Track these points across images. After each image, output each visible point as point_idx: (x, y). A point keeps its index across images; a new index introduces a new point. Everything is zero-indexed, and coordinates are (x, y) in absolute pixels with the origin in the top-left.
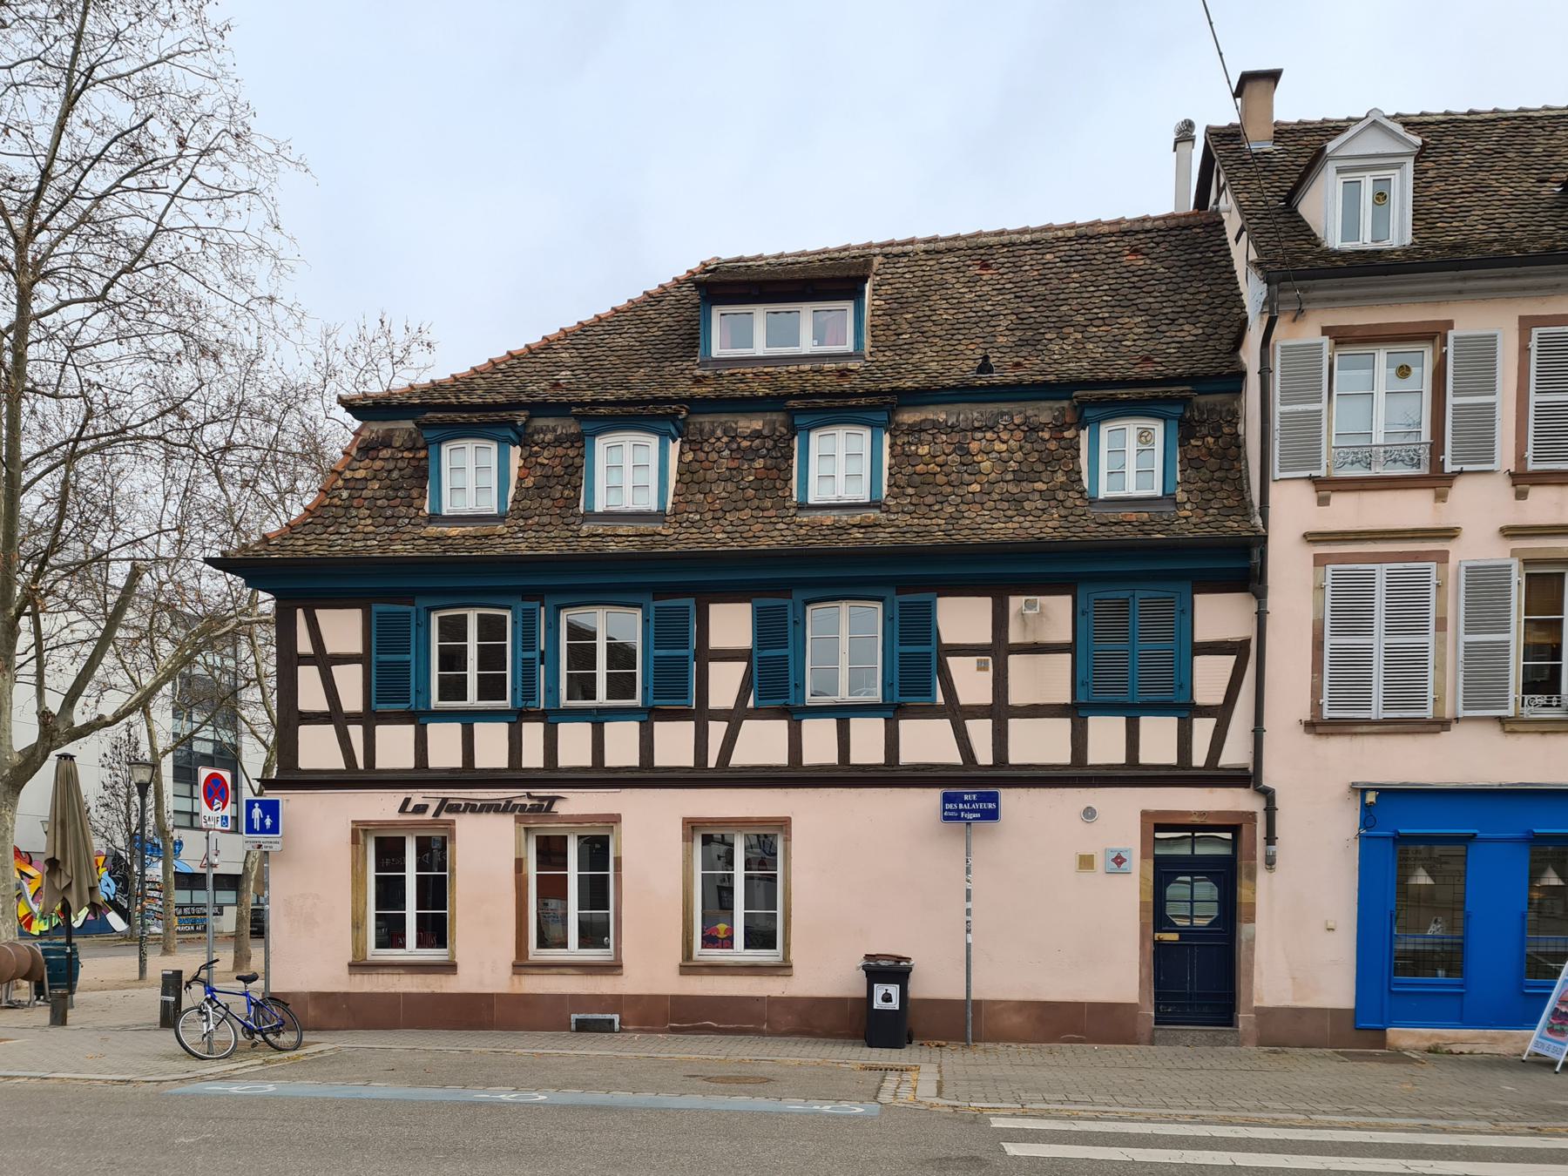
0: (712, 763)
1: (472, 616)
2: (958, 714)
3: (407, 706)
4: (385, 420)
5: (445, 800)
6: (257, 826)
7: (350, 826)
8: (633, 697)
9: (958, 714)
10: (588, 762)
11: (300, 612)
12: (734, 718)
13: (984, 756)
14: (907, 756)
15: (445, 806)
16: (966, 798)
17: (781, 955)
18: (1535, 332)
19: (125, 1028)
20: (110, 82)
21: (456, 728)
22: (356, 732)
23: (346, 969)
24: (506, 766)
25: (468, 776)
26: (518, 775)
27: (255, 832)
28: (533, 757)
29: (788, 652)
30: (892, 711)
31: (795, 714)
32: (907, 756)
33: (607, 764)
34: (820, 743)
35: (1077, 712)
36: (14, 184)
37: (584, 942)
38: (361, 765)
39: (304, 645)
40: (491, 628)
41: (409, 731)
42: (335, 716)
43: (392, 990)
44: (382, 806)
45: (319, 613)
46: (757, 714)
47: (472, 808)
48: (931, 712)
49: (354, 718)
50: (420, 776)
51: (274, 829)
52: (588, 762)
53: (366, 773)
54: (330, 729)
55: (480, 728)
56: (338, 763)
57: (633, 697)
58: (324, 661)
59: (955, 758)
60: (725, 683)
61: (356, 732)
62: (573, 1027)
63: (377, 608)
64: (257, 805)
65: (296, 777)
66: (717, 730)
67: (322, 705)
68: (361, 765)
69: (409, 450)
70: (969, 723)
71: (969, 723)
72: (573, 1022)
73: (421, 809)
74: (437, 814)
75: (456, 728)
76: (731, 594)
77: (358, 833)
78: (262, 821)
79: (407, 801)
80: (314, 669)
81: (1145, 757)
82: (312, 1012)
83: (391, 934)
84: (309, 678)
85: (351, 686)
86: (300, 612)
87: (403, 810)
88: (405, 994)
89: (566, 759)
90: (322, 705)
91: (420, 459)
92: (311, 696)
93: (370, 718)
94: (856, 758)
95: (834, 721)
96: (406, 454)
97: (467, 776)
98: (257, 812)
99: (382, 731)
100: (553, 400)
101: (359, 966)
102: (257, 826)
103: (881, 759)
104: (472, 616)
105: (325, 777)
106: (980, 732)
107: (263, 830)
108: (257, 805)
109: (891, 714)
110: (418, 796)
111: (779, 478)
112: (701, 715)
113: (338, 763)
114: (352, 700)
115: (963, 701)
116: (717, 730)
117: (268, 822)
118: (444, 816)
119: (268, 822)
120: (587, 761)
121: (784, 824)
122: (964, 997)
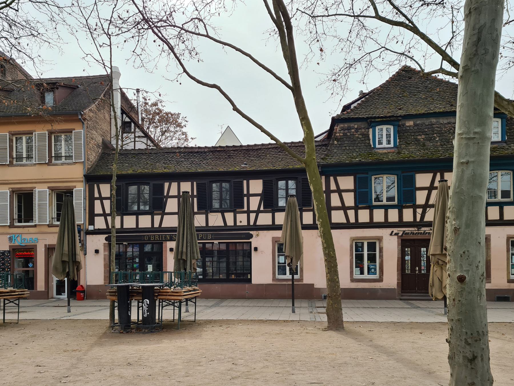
0: (418, 219)
5: (404, 231)
8: (395, 201)
9: (248, 212)
10: (271, 224)
13: (352, 220)
14: (506, 217)
17: (299, 277)
19: (232, 306)
21: (383, 211)
22: (109, 218)
26: (208, 228)
29: (402, 189)
30: (400, 208)
31: (371, 208)
32: (506, 217)
34: (379, 216)
36: (451, 47)
42: (344, 208)
45: (338, 178)
46: (262, 212)
52: (271, 224)
55: (390, 211)
56: (344, 221)
57: (395, 201)
58: (101, 199)
60: (254, 203)
61: (109, 218)
62: (323, 298)
63: (358, 176)
66: (419, 211)
67: (339, 204)
70: (348, 211)
71: (348, 211)
75: (383, 211)
79: (392, 232)
81: (360, 221)
84: (97, 203)
85: (349, 199)
89: (390, 220)
90: (339, 204)
93: (356, 208)
95: (384, 210)
103: (312, 223)
106: (351, 213)
111: (359, 143)
112: (415, 207)
113: (344, 221)
114: (108, 211)
116: (419, 211)
120: (271, 223)
121: (380, 239)
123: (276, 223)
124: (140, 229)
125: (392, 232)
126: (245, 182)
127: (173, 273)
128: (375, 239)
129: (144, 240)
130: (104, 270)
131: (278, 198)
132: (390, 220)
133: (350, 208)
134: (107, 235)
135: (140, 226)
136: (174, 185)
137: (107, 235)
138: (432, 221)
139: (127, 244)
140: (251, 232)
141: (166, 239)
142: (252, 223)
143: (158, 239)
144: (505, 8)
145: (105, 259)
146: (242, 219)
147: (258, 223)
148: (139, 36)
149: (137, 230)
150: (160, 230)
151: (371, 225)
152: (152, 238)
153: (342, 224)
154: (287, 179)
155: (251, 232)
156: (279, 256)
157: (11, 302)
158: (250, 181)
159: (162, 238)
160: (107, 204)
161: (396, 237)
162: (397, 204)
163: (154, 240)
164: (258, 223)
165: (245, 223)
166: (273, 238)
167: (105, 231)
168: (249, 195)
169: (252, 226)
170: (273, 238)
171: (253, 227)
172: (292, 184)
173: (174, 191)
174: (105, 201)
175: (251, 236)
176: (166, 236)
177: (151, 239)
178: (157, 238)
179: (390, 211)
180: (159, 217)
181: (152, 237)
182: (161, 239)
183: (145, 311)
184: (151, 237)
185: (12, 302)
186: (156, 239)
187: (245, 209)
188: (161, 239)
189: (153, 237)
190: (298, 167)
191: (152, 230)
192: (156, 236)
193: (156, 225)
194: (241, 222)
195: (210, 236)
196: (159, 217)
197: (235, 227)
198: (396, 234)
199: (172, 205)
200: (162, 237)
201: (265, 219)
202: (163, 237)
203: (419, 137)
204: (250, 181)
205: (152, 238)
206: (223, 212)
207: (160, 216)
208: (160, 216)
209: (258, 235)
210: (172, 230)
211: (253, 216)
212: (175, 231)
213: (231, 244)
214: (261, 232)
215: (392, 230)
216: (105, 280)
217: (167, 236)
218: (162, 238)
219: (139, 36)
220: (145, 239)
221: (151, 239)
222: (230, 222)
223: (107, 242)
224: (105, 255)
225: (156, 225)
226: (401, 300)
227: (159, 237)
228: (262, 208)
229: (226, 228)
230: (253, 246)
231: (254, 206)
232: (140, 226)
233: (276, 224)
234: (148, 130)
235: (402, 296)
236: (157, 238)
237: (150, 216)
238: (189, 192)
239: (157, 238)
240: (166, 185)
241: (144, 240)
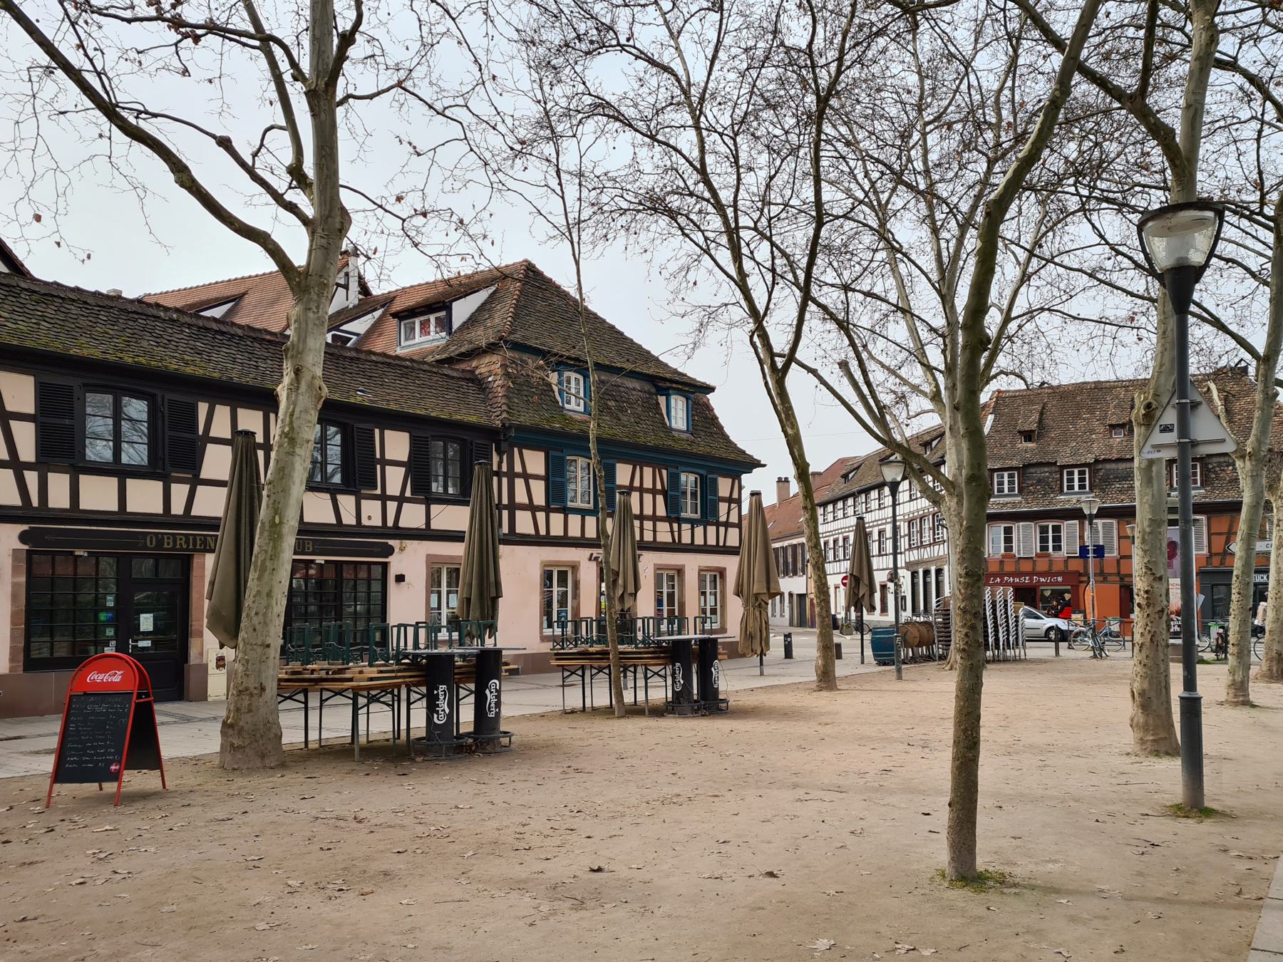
2: (384, 498)
9: (384, 498)
12: (401, 500)
16: (1060, 579)
18: (1065, 471)
20: (776, 252)
22: (31, 478)
26: (77, 515)
28: (591, 532)
31: (566, 511)
33: (128, 510)
35: (196, 481)
38: (35, 503)
39: (518, 468)
42: (532, 508)
46: (409, 500)
48: (375, 497)
58: (526, 477)
59: (17, 501)
60: (395, 479)
67: (526, 501)
68: (35, 503)
77: (439, 571)
79: (592, 555)
80: (522, 480)
86: (516, 449)
89: (520, 529)
90: (526, 501)
93: (548, 509)
97: (692, 547)
114: (540, 499)
115: (398, 494)
116: (722, 529)
123: (83, 506)
124: (435, 533)
125: (592, 555)
126: (377, 431)
127: (651, 621)
128: (551, 566)
129: (145, 547)
130: (12, 629)
131: (85, 437)
133: (29, 466)
134: (25, 527)
135: (131, 508)
136: (222, 413)
137: (25, 527)
138: (220, 519)
139: (86, 555)
140: (391, 542)
141: (205, 546)
142: (390, 523)
143: (185, 547)
145: (14, 597)
146: (372, 513)
147: (193, 513)
149: (122, 516)
150: (188, 521)
151: (564, 541)
152: (168, 544)
153: (529, 535)
154: (446, 439)
155: (391, 542)
156: (449, 593)
157: (286, 698)
158: (218, 407)
159: (195, 544)
161: (595, 563)
163: (173, 549)
165: (377, 522)
166: (428, 556)
167: (20, 513)
168: (385, 463)
170: (428, 556)
171: (392, 532)
172: (137, 408)
173: (221, 427)
175: (389, 551)
176: (206, 539)
177: (166, 546)
178: (181, 544)
180: (185, 488)
181: (168, 538)
182: (191, 547)
183: (442, 698)
184: (166, 540)
185: (290, 698)
186: (178, 547)
187: (378, 492)
188: (191, 547)
189: (171, 541)
190: (418, 412)
191: (165, 519)
192: (178, 537)
193: (177, 508)
194: (370, 518)
195: (310, 546)
196: (185, 488)
197: (359, 529)
198: (596, 559)
199: (218, 462)
200: (195, 541)
201: (413, 516)
202: (199, 542)
203: (609, 403)
204: (218, 407)
205: (168, 544)
206: (334, 492)
207: (188, 487)
208: (188, 487)
209: (402, 550)
210: (212, 524)
211: (392, 506)
212: (216, 528)
213: (63, 558)
214: (408, 543)
216: (12, 660)
217: (209, 538)
218: (195, 544)
220: (148, 543)
221: (166, 546)
222: (349, 519)
223: (27, 547)
224: (14, 585)
225: (177, 508)
227: (187, 542)
228: (408, 494)
229: (339, 528)
230: (393, 572)
231: (394, 488)
232: (131, 508)
233: (128, 510)
236: (183, 542)
237: (161, 484)
238: (253, 434)
239: (181, 544)
240: (203, 408)
241: (145, 547)
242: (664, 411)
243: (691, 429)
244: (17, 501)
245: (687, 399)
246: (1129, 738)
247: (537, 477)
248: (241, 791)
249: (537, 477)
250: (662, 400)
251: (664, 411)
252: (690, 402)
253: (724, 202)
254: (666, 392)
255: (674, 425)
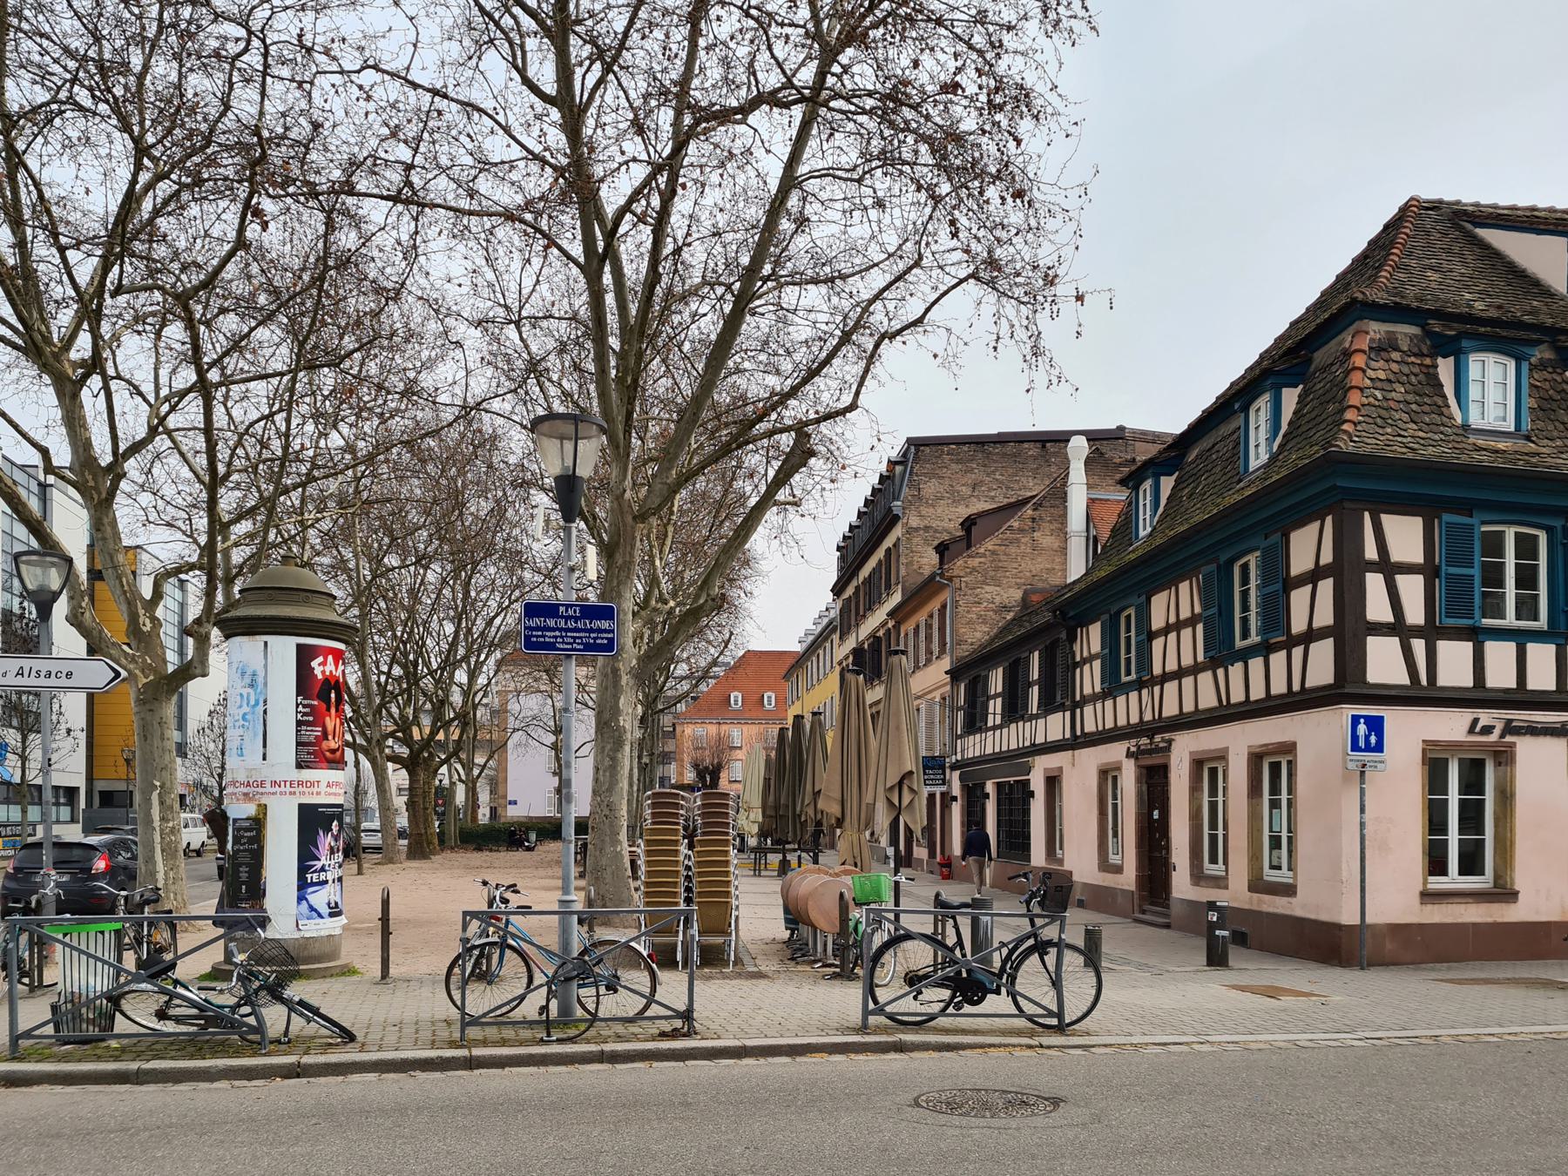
1: (1510, 534)
3: (1470, 622)
4: (1384, 321)
6: (1362, 744)
7: (1420, 746)
11: (1367, 515)
15: (1510, 728)
22: (1419, 646)
23: (1417, 899)
24: (1554, 688)
25: (1520, 698)
27: (1360, 750)
31: (1477, 636)
37: (1463, 871)
38: (1424, 682)
40: (1526, 548)
41: (1467, 647)
42: (1398, 628)
43: (1460, 920)
44: (1451, 725)
47: (1534, 731)
49: (1417, 631)
50: (1477, 697)
51: (1379, 748)
53: (1338, 687)
54: (1394, 642)
55: (1532, 648)
58: (1389, 569)
59: (1404, 680)
61: (1419, 646)
64: (1362, 721)
65: (1365, 691)
66: (1157, 689)
67: (1388, 617)
68: (1424, 682)
69: (1415, 355)
72: (234, 979)
73: (1487, 730)
74: (1502, 736)
75: (1510, 648)
76: (1403, 506)
78: (1367, 738)
79: (1476, 721)
82: (1389, 946)
83: (1436, 864)
84: (1375, 583)
86: (1367, 515)
87: (1471, 731)
88: (1475, 925)
89: (1493, 681)
90: (1388, 617)
91: (1427, 366)
92: (1377, 608)
93: (1432, 632)
94: (1532, 684)
95: (1553, 647)
96: (1413, 359)
97: (1518, 697)
98: (1362, 729)
99: (1442, 646)
100: (1382, 302)
101: (1428, 896)
102: (1362, 744)
104: (1510, 534)
105: (1393, 693)
107: (1368, 748)
108: (1362, 721)
109: (1563, 641)
110: (1486, 717)
114: (1415, 614)
117: (1373, 739)
118: (1508, 739)
119: (1373, 739)
122: (1358, 922)
125: (1476, 721)
132: (1493, 681)
144: (106, 359)
148: (814, 99)
160: (1412, 589)
162: (1546, 628)
164: (1307, 685)
169: (1297, 693)
174: (1402, 580)
179: (1532, 648)
215: (1475, 716)
219: (814, 99)
226: (1137, 921)
234: (232, 485)
235: (1143, 912)
242: (1449, 390)
243: (1527, 425)
244: (1404, 680)
245: (1519, 360)
246: (1104, 935)
247: (1409, 569)
248: (288, 789)
249: (1409, 569)
250: (1445, 369)
251: (1449, 390)
252: (1525, 366)
253: (88, 334)
254: (1453, 348)
255: (1475, 420)
